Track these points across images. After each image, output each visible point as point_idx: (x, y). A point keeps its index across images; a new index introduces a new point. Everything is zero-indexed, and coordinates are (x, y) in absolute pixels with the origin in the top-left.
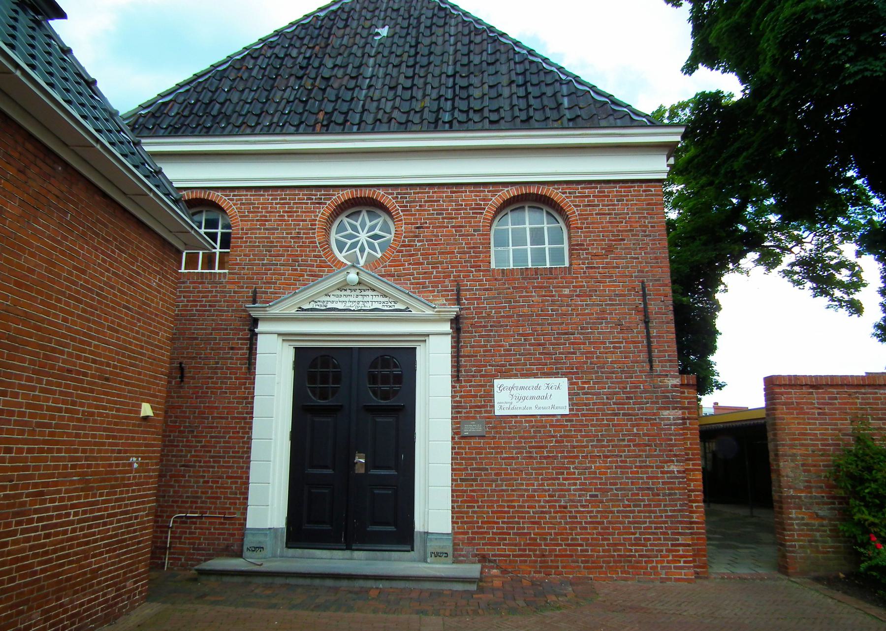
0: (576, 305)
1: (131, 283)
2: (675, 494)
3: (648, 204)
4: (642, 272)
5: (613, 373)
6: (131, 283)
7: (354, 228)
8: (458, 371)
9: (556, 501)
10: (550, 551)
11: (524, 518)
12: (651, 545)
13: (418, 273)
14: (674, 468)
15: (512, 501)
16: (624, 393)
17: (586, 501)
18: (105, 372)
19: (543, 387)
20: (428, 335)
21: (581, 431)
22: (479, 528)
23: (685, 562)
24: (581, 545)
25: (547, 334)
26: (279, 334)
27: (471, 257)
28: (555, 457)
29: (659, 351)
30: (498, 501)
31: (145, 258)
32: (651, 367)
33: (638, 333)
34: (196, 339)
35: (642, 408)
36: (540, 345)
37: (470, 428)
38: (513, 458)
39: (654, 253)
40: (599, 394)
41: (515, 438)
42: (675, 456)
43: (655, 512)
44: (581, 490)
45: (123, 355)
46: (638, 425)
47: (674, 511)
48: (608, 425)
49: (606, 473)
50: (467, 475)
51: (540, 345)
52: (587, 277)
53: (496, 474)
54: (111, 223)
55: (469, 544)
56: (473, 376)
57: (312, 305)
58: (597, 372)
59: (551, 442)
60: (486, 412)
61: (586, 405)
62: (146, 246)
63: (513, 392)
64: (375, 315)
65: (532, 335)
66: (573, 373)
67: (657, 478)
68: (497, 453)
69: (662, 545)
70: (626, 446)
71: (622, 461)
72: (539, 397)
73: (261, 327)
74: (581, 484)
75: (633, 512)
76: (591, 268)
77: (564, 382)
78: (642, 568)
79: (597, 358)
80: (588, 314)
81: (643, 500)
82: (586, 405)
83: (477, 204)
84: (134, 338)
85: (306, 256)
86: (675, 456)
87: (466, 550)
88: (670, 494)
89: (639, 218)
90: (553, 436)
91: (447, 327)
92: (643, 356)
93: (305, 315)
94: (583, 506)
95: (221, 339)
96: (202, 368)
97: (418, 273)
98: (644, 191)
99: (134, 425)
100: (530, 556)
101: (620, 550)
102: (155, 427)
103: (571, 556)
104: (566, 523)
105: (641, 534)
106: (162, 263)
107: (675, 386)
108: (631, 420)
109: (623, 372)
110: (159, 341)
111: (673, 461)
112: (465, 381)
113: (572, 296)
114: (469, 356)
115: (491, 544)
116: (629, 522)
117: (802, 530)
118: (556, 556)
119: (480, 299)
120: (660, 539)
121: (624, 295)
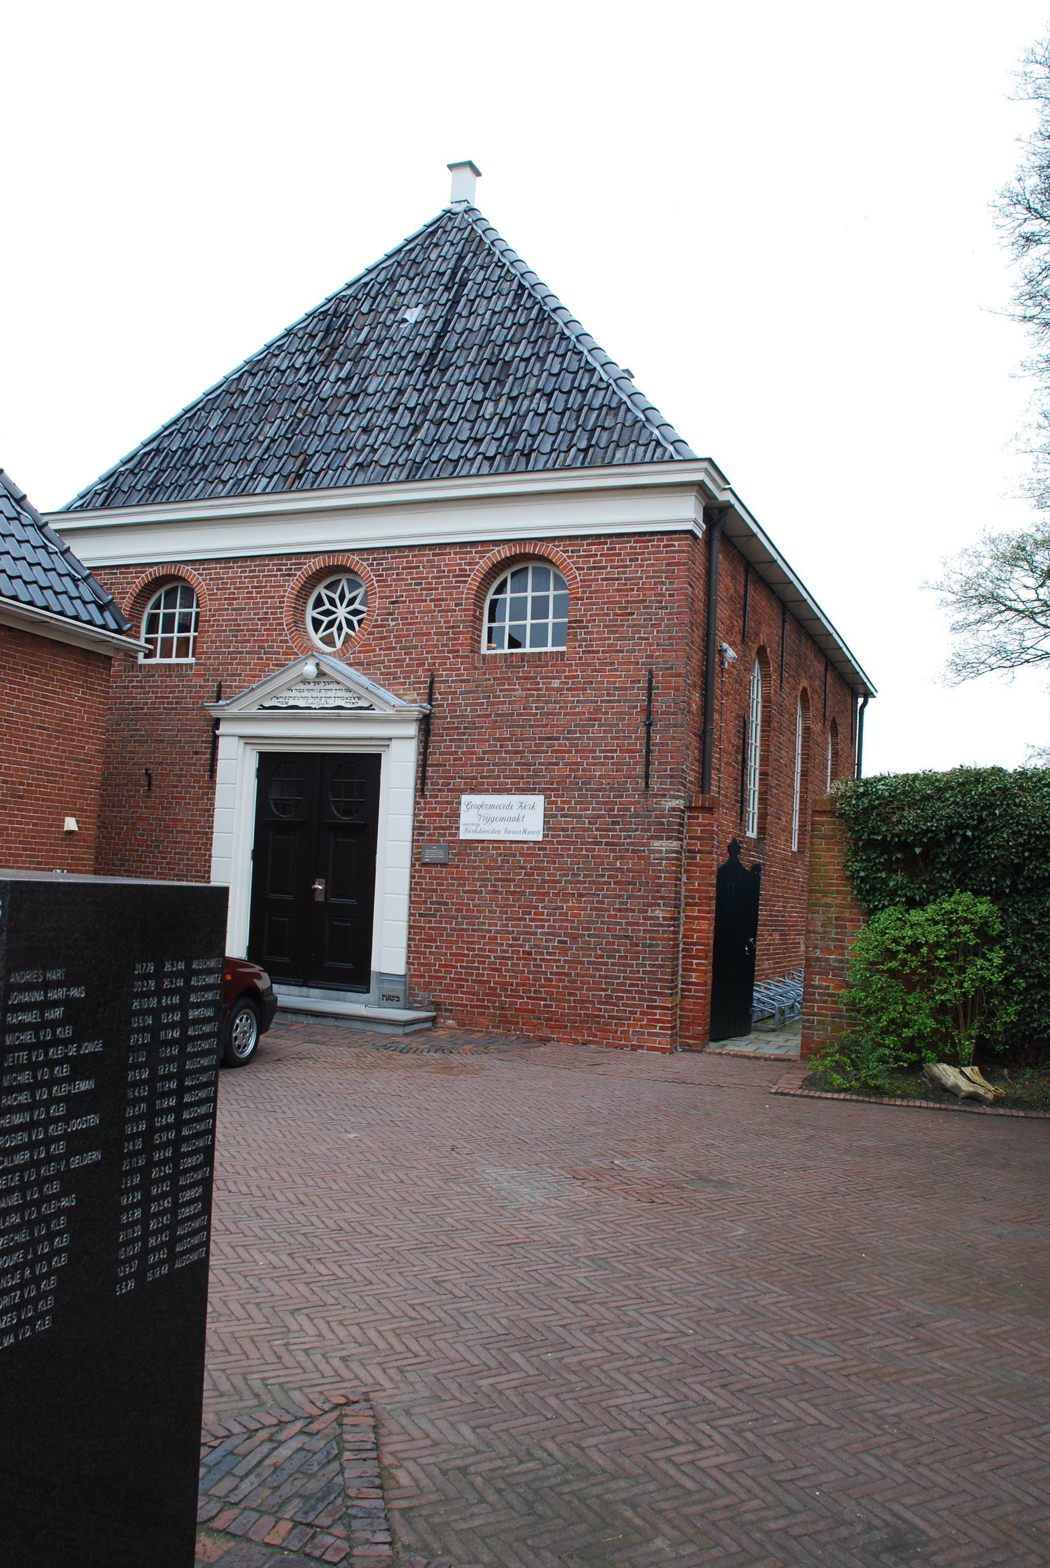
0: (565, 702)
1: (46, 703)
2: (658, 945)
3: (668, 565)
4: (651, 657)
5: (599, 790)
6: (46, 703)
7: (332, 602)
8: (423, 784)
9: (520, 946)
10: (511, 1003)
11: (484, 963)
12: (624, 1005)
13: (389, 661)
14: (659, 913)
15: (473, 943)
16: (610, 816)
17: (554, 947)
18: (19, 790)
19: (516, 806)
20: (390, 739)
21: (554, 862)
22: (436, 971)
23: (661, 1028)
24: (545, 1000)
25: (527, 739)
26: (241, 737)
27: (449, 639)
28: (522, 893)
29: (660, 764)
30: (457, 942)
31: (62, 675)
32: (647, 784)
33: (637, 738)
34: (162, 741)
35: (630, 837)
36: (517, 752)
37: (432, 854)
38: (476, 892)
39: (669, 631)
40: (581, 816)
41: (479, 867)
42: (662, 898)
43: (631, 966)
44: (548, 934)
45: (39, 773)
46: (621, 858)
47: (654, 966)
48: (587, 856)
49: (578, 915)
50: (427, 909)
51: (517, 752)
52: (583, 664)
53: (457, 910)
54: (19, 652)
55: (425, 989)
56: (440, 790)
57: (274, 703)
58: (580, 789)
59: (520, 874)
60: (451, 835)
61: (563, 830)
62: (64, 663)
63: (482, 811)
64: (336, 714)
65: (510, 739)
66: (552, 790)
67: (638, 924)
68: (459, 885)
69: (636, 1006)
70: (605, 883)
71: (598, 902)
72: (510, 819)
73: (224, 729)
74: (549, 927)
75: (606, 964)
76: (589, 652)
77: (539, 800)
78: (611, 1031)
79: (583, 770)
80: (578, 714)
81: (619, 951)
82: (563, 830)
83: (461, 570)
84: (52, 756)
85: (273, 641)
86: (662, 898)
87: (421, 995)
88: (650, 946)
89: (656, 583)
90: (522, 868)
91: (412, 730)
92: (639, 769)
93: (272, 712)
94: (548, 954)
95: (186, 742)
96: (168, 775)
97: (389, 661)
98: (665, 546)
99: (56, 839)
100: (488, 1008)
101: (587, 1008)
102: (85, 841)
103: (534, 1011)
104: (529, 972)
105: (613, 991)
106: (86, 675)
107: (674, 809)
108: (614, 851)
109: (612, 789)
110: (86, 755)
111: (659, 905)
112: (431, 797)
113: (562, 689)
114: (437, 765)
115: (448, 991)
116: (600, 977)
117: (825, 1002)
118: (517, 1010)
119: (455, 693)
120: (634, 998)
121: (626, 689)
